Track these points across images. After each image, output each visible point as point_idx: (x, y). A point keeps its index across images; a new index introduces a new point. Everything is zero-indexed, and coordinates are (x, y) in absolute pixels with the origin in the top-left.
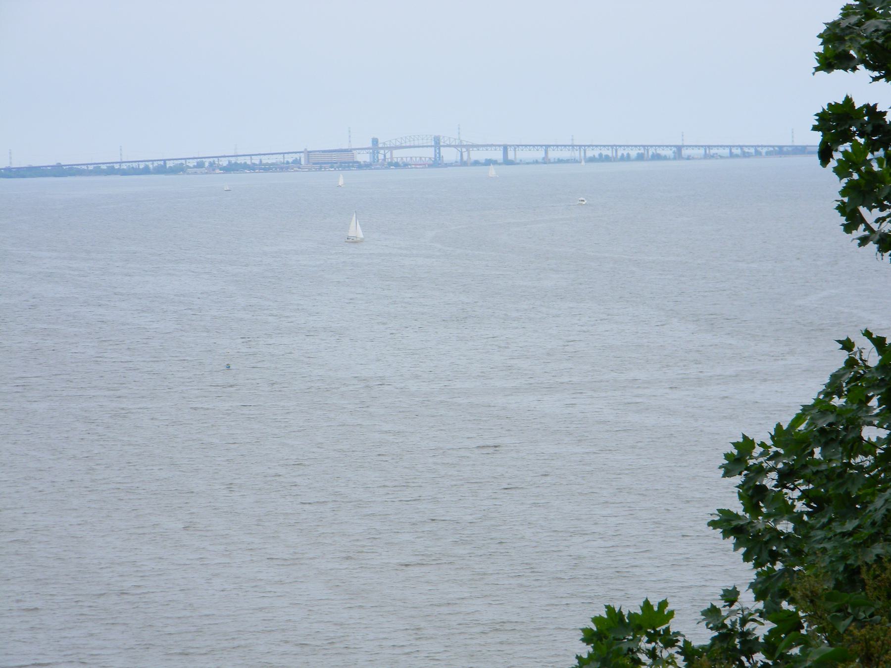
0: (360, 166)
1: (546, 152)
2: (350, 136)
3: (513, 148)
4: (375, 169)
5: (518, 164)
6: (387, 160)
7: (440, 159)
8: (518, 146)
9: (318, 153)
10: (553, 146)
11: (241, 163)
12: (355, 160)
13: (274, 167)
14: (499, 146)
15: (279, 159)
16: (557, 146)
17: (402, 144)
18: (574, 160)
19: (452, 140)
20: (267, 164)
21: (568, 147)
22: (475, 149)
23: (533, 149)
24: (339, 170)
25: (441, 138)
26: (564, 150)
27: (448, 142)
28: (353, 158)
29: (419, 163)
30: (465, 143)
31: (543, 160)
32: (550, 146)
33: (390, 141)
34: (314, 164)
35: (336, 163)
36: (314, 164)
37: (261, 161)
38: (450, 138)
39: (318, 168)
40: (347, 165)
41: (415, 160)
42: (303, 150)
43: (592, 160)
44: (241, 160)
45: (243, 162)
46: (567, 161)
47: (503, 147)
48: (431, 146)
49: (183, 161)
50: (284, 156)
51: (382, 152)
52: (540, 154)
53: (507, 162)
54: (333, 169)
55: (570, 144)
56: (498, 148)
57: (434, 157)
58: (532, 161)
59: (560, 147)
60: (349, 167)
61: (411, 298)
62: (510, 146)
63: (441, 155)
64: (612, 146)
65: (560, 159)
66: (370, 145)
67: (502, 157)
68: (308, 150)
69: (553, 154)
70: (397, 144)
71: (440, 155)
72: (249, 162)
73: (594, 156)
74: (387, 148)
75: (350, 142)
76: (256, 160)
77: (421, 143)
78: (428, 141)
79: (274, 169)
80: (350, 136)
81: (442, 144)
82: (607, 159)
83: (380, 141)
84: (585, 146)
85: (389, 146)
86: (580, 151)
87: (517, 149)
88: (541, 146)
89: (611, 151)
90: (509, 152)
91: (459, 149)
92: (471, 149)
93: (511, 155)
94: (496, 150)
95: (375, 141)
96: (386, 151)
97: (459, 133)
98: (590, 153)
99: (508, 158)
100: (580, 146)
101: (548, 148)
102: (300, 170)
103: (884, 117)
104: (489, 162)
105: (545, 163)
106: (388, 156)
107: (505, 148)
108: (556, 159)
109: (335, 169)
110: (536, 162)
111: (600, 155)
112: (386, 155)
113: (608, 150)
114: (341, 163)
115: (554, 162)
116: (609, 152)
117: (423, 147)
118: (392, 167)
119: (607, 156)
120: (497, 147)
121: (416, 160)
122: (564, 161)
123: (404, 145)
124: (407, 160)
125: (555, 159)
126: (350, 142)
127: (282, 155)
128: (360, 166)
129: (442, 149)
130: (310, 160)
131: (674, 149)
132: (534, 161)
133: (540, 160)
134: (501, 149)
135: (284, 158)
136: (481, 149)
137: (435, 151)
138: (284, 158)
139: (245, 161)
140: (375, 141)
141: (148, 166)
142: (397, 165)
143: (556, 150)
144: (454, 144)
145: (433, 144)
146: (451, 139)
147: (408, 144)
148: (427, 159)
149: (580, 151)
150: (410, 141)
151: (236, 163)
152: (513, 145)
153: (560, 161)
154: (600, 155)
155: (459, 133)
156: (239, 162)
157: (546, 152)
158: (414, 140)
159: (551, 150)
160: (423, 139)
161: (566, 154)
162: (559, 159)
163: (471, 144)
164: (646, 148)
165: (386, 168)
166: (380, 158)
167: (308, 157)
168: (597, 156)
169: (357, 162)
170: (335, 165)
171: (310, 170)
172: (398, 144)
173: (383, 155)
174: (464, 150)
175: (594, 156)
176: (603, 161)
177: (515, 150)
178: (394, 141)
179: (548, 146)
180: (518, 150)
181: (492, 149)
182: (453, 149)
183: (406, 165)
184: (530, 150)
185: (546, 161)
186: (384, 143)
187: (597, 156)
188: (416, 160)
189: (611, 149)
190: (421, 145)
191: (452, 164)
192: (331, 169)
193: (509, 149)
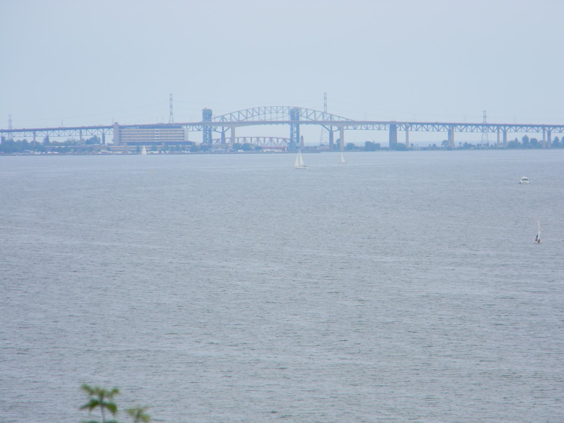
0: (194, 148)
1: (451, 133)
2: (171, 107)
3: (404, 126)
4: (216, 153)
5: (411, 149)
6: (236, 140)
7: (298, 141)
8: (411, 124)
9: (134, 129)
10: (461, 125)
11: (19, 141)
12: (185, 140)
13: (72, 148)
14: (385, 123)
15: (76, 136)
16: (466, 125)
17: (247, 118)
18: (488, 144)
19: (318, 114)
20: (55, 143)
21: (426, 126)
22: (350, 127)
23: (431, 129)
24: (165, 153)
25: (303, 110)
26: (531, 130)
27: (312, 117)
28: (184, 137)
29: (269, 146)
30: (336, 119)
31: (442, 145)
32: (455, 125)
33: (231, 114)
34: (129, 144)
35: (159, 144)
36: (129, 144)
37: (47, 139)
38: (315, 111)
39: (135, 149)
40: (175, 146)
41: (263, 142)
42: (110, 124)
43: (514, 145)
44: (18, 137)
45: (21, 139)
46: (479, 147)
47: (389, 126)
48: (286, 122)
49: (98, 133)
50: (64, 135)
51: (219, 129)
52: (441, 136)
53: (395, 146)
54: (157, 152)
55: (481, 121)
56: (383, 127)
57: (289, 137)
58: (427, 146)
59: (470, 127)
60: (178, 149)
61: (253, 349)
62: (401, 124)
63: (301, 134)
64: (543, 126)
65: (468, 143)
66: (200, 119)
67: (328, 141)
68: (121, 123)
69: (460, 137)
70: (241, 119)
71: (298, 135)
72: (30, 140)
73: (516, 139)
74: (227, 124)
75: (171, 114)
76: (40, 139)
77: (274, 117)
78: (285, 114)
79: (72, 150)
80: (171, 107)
81: (302, 119)
82: (533, 144)
83: (214, 114)
84: (505, 125)
85: (229, 121)
86: (498, 132)
87: (410, 129)
88: (444, 125)
89: (542, 134)
90: (398, 132)
91: (328, 127)
92: (345, 128)
93: (401, 137)
94: (379, 129)
95: (207, 114)
96: (225, 128)
97: (325, 105)
98: (512, 136)
99: (397, 142)
100: (499, 126)
101: (453, 128)
102: (111, 152)
103: (529, 140)
104: (371, 147)
105: (449, 149)
106: (228, 134)
107: (393, 127)
108: (463, 143)
109: (160, 151)
110: (434, 147)
111: (525, 139)
112: (225, 133)
113: (538, 131)
114: (167, 143)
115: (460, 148)
116: (539, 136)
117: (277, 123)
118: (239, 151)
119: (534, 141)
120: (381, 125)
121: (278, 141)
122: (474, 146)
123: (250, 120)
124: (251, 141)
125: (460, 143)
126: (171, 114)
127: (79, 131)
128: (194, 148)
129: (301, 126)
130: (123, 139)
131: (221, 117)
132: (430, 145)
133: (439, 145)
134: (112, 133)
135: (81, 135)
136: (359, 127)
137: (292, 129)
138: (81, 135)
139: (25, 138)
140: (207, 114)
141: (26, 141)
142: (247, 148)
143: (464, 130)
144: (320, 119)
145: (287, 118)
146: (309, 111)
147: (256, 119)
148: (280, 141)
149: (498, 132)
150: (259, 114)
151: (11, 142)
152: (405, 123)
153: (467, 146)
154: (525, 139)
155: (325, 105)
156: (15, 140)
157: (451, 133)
158: (271, 113)
159: (457, 130)
160: (277, 112)
161: (475, 137)
162: (466, 143)
163: (344, 120)
164: (503, 128)
165: (232, 152)
166: (213, 138)
167: (120, 134)
168: (520, 140)
169: (189, 143)
170: (158, 146)
171: (124, 153)
172: (242, 118)
173: (221, 134)
174: (335, 128)
175: (516, 139)
176: (530, 148)
177: (406, 129)
178: (236, 115)
179: (453, 125)
180: (400, 130)
181: (375, 128)
182: (320, 127)
183: (259, 149)
184: (59, 136)
185: (448, 146)
186: (223, 117)
187: (520, 140)
188: (278, 141)
189: (542, 131)
190: (275, 120)
191: (316, 147)
192: (154, 152)
193: (398, 129)
